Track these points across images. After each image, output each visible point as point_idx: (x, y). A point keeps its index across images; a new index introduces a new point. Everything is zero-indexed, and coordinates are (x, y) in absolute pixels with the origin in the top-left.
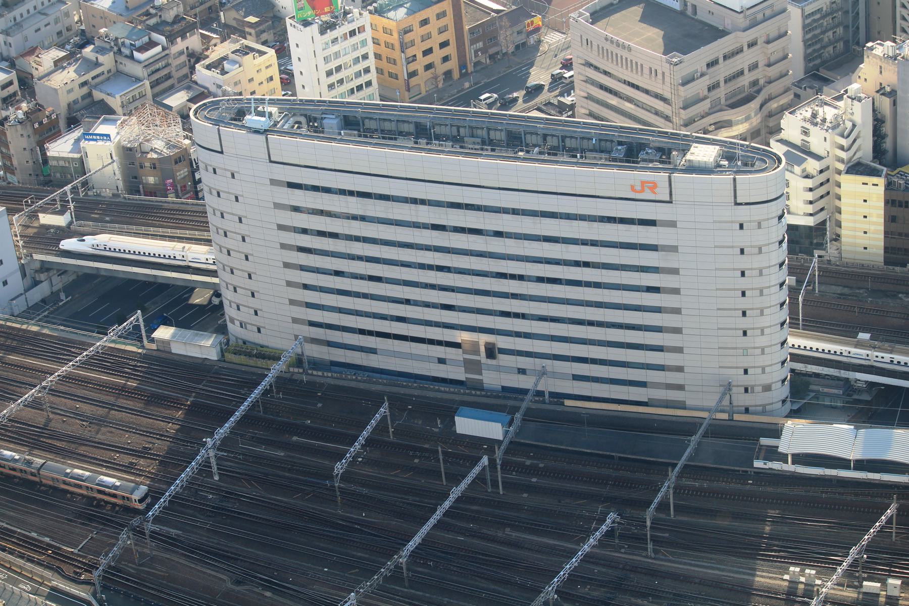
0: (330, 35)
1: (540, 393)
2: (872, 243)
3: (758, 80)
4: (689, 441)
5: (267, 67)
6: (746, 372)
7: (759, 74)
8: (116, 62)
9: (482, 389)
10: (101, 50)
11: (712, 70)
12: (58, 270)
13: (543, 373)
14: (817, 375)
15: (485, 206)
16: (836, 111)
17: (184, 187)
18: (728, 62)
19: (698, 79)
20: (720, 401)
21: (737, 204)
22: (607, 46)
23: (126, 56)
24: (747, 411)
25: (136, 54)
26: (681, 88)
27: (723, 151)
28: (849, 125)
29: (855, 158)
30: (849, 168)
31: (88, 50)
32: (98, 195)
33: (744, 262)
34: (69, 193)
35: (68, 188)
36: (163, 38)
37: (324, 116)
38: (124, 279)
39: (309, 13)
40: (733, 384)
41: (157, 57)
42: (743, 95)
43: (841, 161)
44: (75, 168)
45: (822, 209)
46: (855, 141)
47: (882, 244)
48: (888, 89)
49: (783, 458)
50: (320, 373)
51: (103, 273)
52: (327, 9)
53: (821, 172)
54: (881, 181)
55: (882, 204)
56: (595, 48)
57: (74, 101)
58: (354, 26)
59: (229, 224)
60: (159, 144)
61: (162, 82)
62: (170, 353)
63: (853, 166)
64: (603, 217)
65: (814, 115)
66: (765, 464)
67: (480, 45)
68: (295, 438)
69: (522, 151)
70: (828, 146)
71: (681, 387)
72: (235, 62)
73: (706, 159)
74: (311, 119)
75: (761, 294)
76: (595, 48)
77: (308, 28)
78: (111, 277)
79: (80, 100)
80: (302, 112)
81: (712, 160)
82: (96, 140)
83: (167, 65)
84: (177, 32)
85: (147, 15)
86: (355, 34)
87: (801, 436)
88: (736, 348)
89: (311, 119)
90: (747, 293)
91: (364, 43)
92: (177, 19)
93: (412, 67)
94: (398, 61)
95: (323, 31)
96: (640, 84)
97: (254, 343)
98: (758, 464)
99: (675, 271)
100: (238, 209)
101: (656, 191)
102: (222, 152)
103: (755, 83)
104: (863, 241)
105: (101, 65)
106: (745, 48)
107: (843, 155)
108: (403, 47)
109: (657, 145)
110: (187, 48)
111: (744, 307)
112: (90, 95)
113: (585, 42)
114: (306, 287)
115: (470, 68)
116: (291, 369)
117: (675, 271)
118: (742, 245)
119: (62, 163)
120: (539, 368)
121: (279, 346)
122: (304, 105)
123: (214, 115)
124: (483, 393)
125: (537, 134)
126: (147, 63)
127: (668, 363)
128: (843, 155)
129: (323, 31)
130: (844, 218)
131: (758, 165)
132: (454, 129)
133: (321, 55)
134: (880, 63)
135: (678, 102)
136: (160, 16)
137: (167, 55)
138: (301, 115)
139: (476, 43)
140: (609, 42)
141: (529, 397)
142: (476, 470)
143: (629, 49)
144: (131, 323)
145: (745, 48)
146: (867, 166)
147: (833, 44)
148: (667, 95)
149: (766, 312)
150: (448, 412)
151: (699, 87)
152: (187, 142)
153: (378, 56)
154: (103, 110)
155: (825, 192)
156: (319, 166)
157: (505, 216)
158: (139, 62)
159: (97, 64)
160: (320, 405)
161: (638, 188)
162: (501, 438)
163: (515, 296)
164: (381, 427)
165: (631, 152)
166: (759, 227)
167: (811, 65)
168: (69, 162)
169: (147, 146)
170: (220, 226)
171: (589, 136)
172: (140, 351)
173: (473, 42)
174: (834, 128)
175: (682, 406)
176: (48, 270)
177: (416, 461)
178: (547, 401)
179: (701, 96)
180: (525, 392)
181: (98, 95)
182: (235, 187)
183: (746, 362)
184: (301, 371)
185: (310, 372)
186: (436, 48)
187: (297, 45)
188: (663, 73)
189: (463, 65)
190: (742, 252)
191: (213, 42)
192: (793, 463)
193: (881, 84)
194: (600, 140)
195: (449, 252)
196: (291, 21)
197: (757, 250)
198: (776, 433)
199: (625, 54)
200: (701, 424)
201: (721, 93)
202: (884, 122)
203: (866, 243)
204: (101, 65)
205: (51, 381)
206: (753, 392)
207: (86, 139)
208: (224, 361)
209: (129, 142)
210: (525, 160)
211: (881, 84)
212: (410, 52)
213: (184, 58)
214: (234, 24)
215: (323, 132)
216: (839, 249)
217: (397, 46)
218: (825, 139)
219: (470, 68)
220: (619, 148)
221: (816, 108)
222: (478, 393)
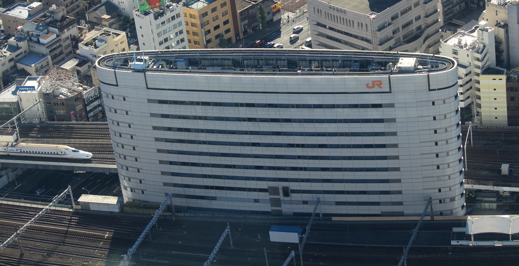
0: (161, 20)
1: (318, 215)
2: (500, 114)
3: (421, 26)
4: (412, 232)
5: (121, 43)
6: (440, 191)
7: (421, 23)
8: (29, 46)
9: (282, 215)
10: (19, 39)
11: (394, 21)
12: (12, 168)
13: (318, 202)
14: (480, 191)
15: (280, 104)
16: (473, 38)
17: (81, 116)
18: (403, 16)
19: (387, 27)
20: (426, 208)
21: (430, 90)
22: (331, 12)
23: (35, 42)
24: (441, 214)
25: (42, 40)
26: (378, 33)
27: (419, 61)
28: (481, 46)
29: (486, 65)
30: (483, 71)
31: (12, 40)
32: (31, 123)
33: (436, 125)
34: (15, 122)
35: (15, 118)
36: (57, 30)
37: (176, 60)
38: (53, 170)
39: (147, 7)
40: (433, 198)
41: (54, 41)
42: (412, 36)
43: (478, 67)
44: (14, 108)
45: (468, 98)
46: (485, 55)
47: (506, 114)
48: (502, 24)
49: (468, 237)
50: (183, 215)
51: (40, 168)
52: (157, 4)
53: (466, 75)
54: (504, 77)
55: (505, 91)
56: (323, 14)
57: (6, 71)
58: (174, 14)
59: (123, 129)
60: (64, 90)
61: (58, 56)
62: (90, 210)
63: (486, 70)
64: (351, 105)
65: (460, 43)
66: (458, 242)
67: (246, 22)
68: (173, 252)
69: (300, 69)
70: (469, 59)
71: (400, 203)
72: (101, 41)
73: (410, 66)
74: (168, 61)
75: (447, 143)
76: (323, 14)
77: (148, 16)
78: (45, 170)
79: (9, 69)
80: (163, 58)
81: (413, 66)
82: (26, 90)
83: (60, 46)
84: (65, 25)
85: (45, 17)
86: (175, 19)
87: (479, 224)
88: (433, 177)
89: (168, 61)
90: (439, 143)
91: (180, 24)
92: (64, 18)
93: (209, 37)
94: (200, 34)
95: (156, 18)
96: (352, 33)
97: (140, 201)
98: (454, 243)
99: (394, 134)
100: (128, 119)
101: (382, 86)
102: (117, 85)
103: (419, 28)
104: (495, 113)
105: (20, 48)
106: (413, 7)
107: (479, 64)
108: (203, 25)
109: (378, 60)
110: (71, 35)
111: (437, 151)
112: (15, 66)
113: (316, 11)
114: (171, 163)
115: (242, 36)
116: (165, 214)
117: (394, 134)
118: (434, 114)
119: (6, 106)
120: (316, 200)
121: (155, 201)
122: (163, 54)
123: (111, 63)
124: (283, 217)
125: (306, 60)
126: (48, 45)
127: (392, 189)
128: (479, 64)
129: (156, 18)
130: (482, 102)
131: (441, 66)
132: (256, 62)
133: (156, 32)
134: (496, 9)
135: (376, 41)
136: (53, 17)
137: (59, 40)
138: (162, 60)
139: (244, 21)
140: (332, 10)
141: (312, 218)
142: (289, 259)
143: (345, 12)
144: (65, 193)
145: (413, 7)
146: (494, 69)
147: (459, 4)
148: (369, 38)
149: (450, 153)
150: (265, 231)
151: (388, 32)
152: (81, 88)
153: (188, 32)
154: (24, 74)
155: (471, 85)
156: (177, 88)
157: (292, 109)
158: (44, 45)
159: (18, 48)
160: (185, 232)
161: (371, 85)
162: (298, 242)
163: (299, 157)
164: (226, 242)
165: (364, 65)
166: (444, 103)
167: (447, 17)
168: (10, 105)
169: (57, 92)
170: (117, 130)
171: (337, 58)
172: (71, 210)
173: (242, 20)
174: (473, 49)
175: (402, 214)
176: (6, 168)
177: (249, 259)
178: (321, 219)
179: (389, 37)
180: (309, 214)
181: (20, 66)
182: (126, 105)
183: (438, 185)
184: (171, 214)
185: (176, 214)
186: (221, 25)
187: (141, 27)
188: (367, 25)
189: (237, 35)
190: (435, 118)
191: (84, 31)
192: (475, 240)
193: (497, 21)
194: (344, 61)
195: (259, 134)
196: (137, 13)
197: (443, 117)
198: (463, 223)
199: (342, 15)
200: (417, 224)
201: (400, 34)
202: (501, 43)
203: (496, 114)
204: (20, 48)
205: (22, 230)
206: (444, 202)
207: (20, 90)
208: (123, 212)
209: (47, 90)
210: (302, 74)
211: (497, 21)
212: (207, 28)
213: (69, 41)
214: (95, 20)
215: (177, 68)
216: (481, 120)
217: (199, 26)
218: (468, 55)
219: (242, 36)
220: (356, 64)
221: (461, 38)
222: (280, 218)
